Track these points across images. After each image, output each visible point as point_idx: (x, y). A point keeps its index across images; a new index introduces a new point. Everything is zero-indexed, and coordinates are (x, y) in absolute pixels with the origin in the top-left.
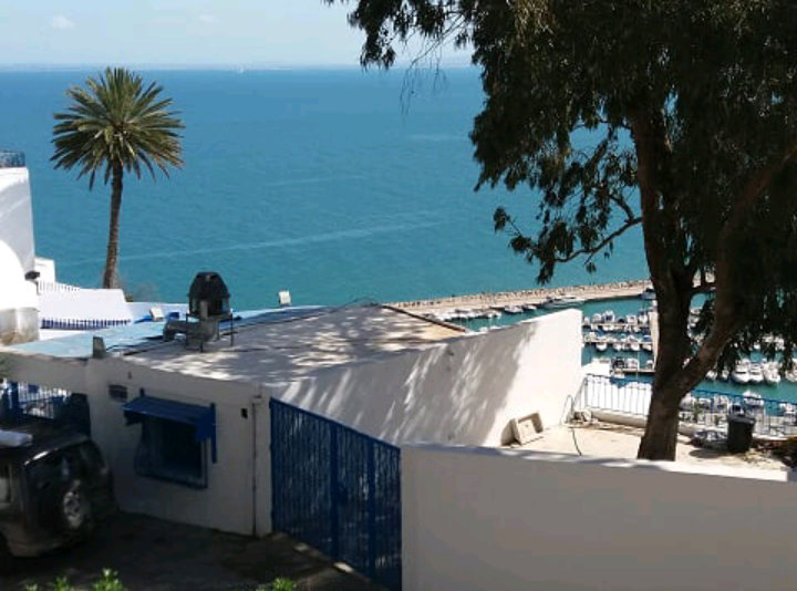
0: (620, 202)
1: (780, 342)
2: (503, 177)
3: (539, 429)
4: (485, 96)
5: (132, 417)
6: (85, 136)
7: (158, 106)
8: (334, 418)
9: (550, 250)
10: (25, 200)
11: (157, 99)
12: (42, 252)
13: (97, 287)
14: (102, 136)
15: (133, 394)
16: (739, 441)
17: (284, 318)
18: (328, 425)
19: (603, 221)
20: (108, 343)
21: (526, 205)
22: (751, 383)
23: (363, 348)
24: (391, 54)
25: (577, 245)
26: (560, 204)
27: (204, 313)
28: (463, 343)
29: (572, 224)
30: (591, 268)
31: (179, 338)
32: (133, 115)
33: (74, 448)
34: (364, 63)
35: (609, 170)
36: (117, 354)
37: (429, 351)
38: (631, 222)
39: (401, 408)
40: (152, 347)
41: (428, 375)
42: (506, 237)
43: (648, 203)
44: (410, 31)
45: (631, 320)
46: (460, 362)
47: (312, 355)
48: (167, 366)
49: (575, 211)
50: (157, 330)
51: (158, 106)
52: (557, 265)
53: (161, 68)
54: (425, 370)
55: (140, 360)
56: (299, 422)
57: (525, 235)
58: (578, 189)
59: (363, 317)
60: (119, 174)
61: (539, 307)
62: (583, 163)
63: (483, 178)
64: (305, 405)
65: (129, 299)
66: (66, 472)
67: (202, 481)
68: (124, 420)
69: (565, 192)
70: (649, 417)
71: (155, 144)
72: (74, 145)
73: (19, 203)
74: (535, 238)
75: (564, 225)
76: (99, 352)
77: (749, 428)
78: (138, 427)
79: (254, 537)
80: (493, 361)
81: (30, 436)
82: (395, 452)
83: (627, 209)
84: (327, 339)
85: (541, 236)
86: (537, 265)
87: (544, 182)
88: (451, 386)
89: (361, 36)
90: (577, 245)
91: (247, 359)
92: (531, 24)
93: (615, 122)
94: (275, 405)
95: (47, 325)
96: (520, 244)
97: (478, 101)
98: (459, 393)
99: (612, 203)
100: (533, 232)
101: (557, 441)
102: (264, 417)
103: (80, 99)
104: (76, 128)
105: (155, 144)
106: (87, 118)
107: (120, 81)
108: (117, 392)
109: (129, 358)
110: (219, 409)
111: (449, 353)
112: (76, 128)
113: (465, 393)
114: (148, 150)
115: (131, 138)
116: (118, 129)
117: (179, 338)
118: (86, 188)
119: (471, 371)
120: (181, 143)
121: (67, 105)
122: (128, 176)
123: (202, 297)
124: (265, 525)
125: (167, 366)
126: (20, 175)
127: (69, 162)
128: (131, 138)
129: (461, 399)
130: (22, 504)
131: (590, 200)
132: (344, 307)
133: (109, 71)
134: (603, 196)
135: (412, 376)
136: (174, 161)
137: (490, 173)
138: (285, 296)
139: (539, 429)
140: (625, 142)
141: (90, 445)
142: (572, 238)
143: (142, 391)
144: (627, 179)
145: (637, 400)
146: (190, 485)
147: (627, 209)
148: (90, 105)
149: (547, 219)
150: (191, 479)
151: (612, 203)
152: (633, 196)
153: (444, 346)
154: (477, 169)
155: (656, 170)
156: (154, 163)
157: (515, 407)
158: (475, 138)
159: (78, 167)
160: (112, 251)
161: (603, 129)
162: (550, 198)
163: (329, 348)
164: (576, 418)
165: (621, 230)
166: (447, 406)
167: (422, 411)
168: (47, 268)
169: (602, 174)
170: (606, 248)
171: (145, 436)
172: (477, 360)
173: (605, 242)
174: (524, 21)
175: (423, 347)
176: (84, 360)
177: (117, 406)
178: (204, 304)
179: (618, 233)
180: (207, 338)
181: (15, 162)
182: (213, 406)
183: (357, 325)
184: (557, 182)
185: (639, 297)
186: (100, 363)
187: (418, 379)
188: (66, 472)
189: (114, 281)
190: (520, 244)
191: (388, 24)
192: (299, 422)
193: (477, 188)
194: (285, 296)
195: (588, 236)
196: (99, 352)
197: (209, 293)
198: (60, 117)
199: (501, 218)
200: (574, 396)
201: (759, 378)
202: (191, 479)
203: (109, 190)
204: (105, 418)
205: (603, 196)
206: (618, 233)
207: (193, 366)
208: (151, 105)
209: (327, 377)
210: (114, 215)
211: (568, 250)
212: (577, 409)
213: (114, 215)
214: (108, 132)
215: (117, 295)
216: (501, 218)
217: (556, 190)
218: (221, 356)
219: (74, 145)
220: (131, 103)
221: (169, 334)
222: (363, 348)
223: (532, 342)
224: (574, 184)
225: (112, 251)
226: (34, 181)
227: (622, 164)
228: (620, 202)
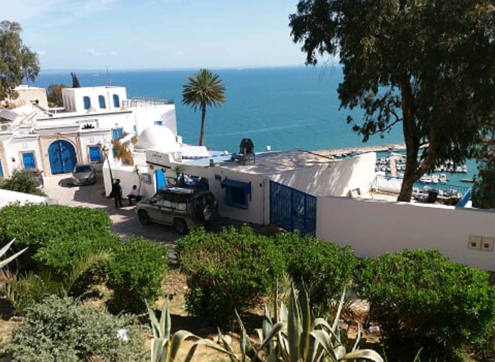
0: (394, 113)
1: (452, 163)
2: (349, 105)
3: (359, 193)
4: (343, 76)
5: (223, 186)
6: (193, 93)
7: (218, 82)
8: (291, 187)
9: (367, 131)
10: (174, 116)
11: (217, 80)
12: (178, 134)
13: (196, 145)
14: (199, 94)
15: (223, 178)
16: (432, 198)
17: (270, 155)
18: (290, 190)
19: (387, 120)
20: (215, 161)
21: (359, 114)
22: (427, 183)
23: (299, 164)
24: (316, 61)
25: (377, 129)
26: (371, 114)
27: (245, 152)
28: (334, 164)
29: (376, 121)
30: (382, 137)
31: (237, 160)
32: (209, 85)
33: (207, 194)
34: (306, 64)
35: (390, 102)
36: (217, 165)
37: (322, 166)
38: (398, 120)
39: (312, 185)
40: (226, 163)
41: (322, 174)
42: (351, 126)
43: (405, 114)
44: (324, 53)
45: (383, 160)
46: (332, 172)
47: (282, 167)
48: (234, 169)
49: (378, 116)
50: (229, 158)
51: (218, 82)
52: (370, 136)
53: (253, 68)
54: (321, 173)
55: (225, 167)
56: (279, 188)
57: (358, 125)
58: (378, 109)
59: (297, 154)
60: (204, 106)
61: (348, 154)
62: (381, 99)
63: (341, 106)
64: (281, 182)
65: (208, 150)
66: (204, 202)
67: (245, 207)
68: (220, 187)
69: (374, 110)
70: (402, 190)
71: (217, 96)
72: (190, 97)
73: (172, 117)
74: (361, 127)
75: (373, 122)
76: (212, 165)
77: (437, 194)
78: (224, 189)
79: (263, 226)
80: (344, 170)
81: (193, 191)
82: (315, 198)
83: (396, 116)
84: (286, 162)
85: (364, 126)
86: (362, 136)
87: (366, 106)
88: (329, 178)
89: (305, 54)
90: (377, 129)
91: (261, 168)
92: (368, 49)
93: (393, 84)
94: (271, 182)
95: (183, 158)
96: (356, 128)
97: (340, 78)
98: (332, 181)
99: (391, 114)
100: (361, 124)
101: (365, 195)
102: (268, 186)
103: (191, 80)
104: (190, 90)
105: (217, 96)
106: (194, 87)
107: (205, 73)
108: (218, 177)
109: (222, 167)
110: (252, 184)
111: (329, 166)
112: (190, 90)
113: (334, 181)
114: (214, 98)
115: (208, 94)
116: (204, 90)
117: (237, 160)
118: (193, 110)
119: (336, 174)
120: (224, 95)
121: (187, 82)
122: (207, 107)
123: (244, 147)
124: (267, 221)
125: (234, 169)
126: (172, 107)
127: (188, 102)
128: (208, 94)
129: (332, 183)
130: (191, 212)
131: (383, 113)
132: (290, 151)
133: (201, 70)
134: (387, 111)
135: (316, 175)
136: (223, 102)
137: (344, 104)
138: (269, 148)
139: (359, 193)
140: (397, 92)
141: (211, 193)
142: (375, 127)
143: (226, 178)
144: (397, 105)
145: (397, 185)
146: (241, 208)
147: (396, 116)
148: (195, 82)
149: (367, 120)
150: (242, 206)
151: (391, 114)
152: (399, 112)
153: (327, 164)
154: (340, 102)
155: (410, 104)
156: (216, 102)
157: (351, 185)
158: (339, 91)
159: (191, 104)
160: (202, 133)
161: (389, 88)
162: (368, 112)
163: (287, 164)
164: (372, 190)
165: (394, 123)
166: (327, 185)
167: (319, 187)
168: (180, 139)
169: (387, 103)
170: (388, 129)
171: (227, 193)
172: (339, 170)
173: (387, 128)
174: (366, 49)
175: (320, 164)
176: (207, 167)
177: (218, 182)
178: (245, 149)
179: (392, 125)
180: (246, 160)
181: (170, 102)
182: (250, 183)
183: (296, 157)
184: (370, 106)
185: (386, 151)
186: (212, 168)
187: (318, 175)
188: (204, 202)
189: (203, 143)
190: (356, 128)
191: (316, 50)
192: (279, 188)
193: (339, 109)
194: (269, 148)
195: (381, 126)
196: (212, 165)
197: (247, 146)
198: (185, 86)
199: (349, 119)
200: (372, 182)
201: (430, 181)
202: (242, 206)
203: (201, 112)
204: (214, 186)
205: (387, 111)
206: (392, 125)
207: (243, 170)
208: (215, 82)
209: (286, 175)
210: (203, 121)
211: (374, 131)
212: (373, 187)
213: (203, 121)
214: (201, 91)
215: (204, 148)
216: (349, 119)
217: (371, 109)
218: (252, 167)
219: (190, 97)
220: (208, 81)
221: (233, 159)
222: (299, 164)
223: (358, 163)
224: (377, 107)
225: (202, 133)
226: (178, 112)
227: (395, 99)
228: (394, 113)
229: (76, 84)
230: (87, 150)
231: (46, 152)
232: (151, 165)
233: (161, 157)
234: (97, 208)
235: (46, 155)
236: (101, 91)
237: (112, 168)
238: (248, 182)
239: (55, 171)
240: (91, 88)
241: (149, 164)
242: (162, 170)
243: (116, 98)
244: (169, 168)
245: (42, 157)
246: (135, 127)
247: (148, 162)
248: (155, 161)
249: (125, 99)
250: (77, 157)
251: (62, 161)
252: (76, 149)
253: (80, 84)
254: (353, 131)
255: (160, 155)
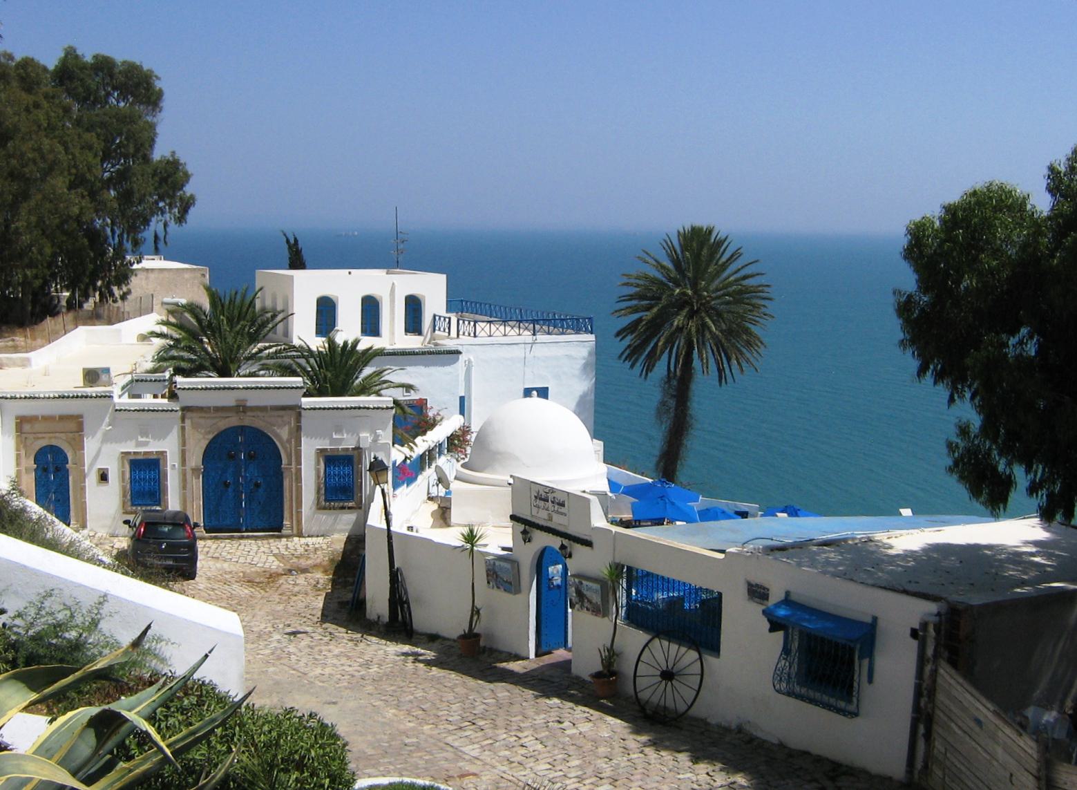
15: (776, 596)
67: (852, 708)
181: (577, 325)
182: (875, 619)
202: (842, 704)
229: (297, 262)
230: (318, 463)
231: (196, 459)
232: (525, 525)
233: (562, 505)
234: (146, 732)
235: (194, 470)
236: (373, 281)
237: (398, 527)
238: (869, 620)
239: (215, 523)
240: (344, 272)
241: (521, 527)
242: (563, 547)
243: (414, 306)
244: (588, 544)
245: (184, 474)
246: (462, 399)
247: (513, 518)
248: (541, 517)
249: (442, 311)
250: (286, 483)
251: (238, 494)
252: (284, 461)
253: (306, 254)
254: (171, 150)
255: (561, 498)
